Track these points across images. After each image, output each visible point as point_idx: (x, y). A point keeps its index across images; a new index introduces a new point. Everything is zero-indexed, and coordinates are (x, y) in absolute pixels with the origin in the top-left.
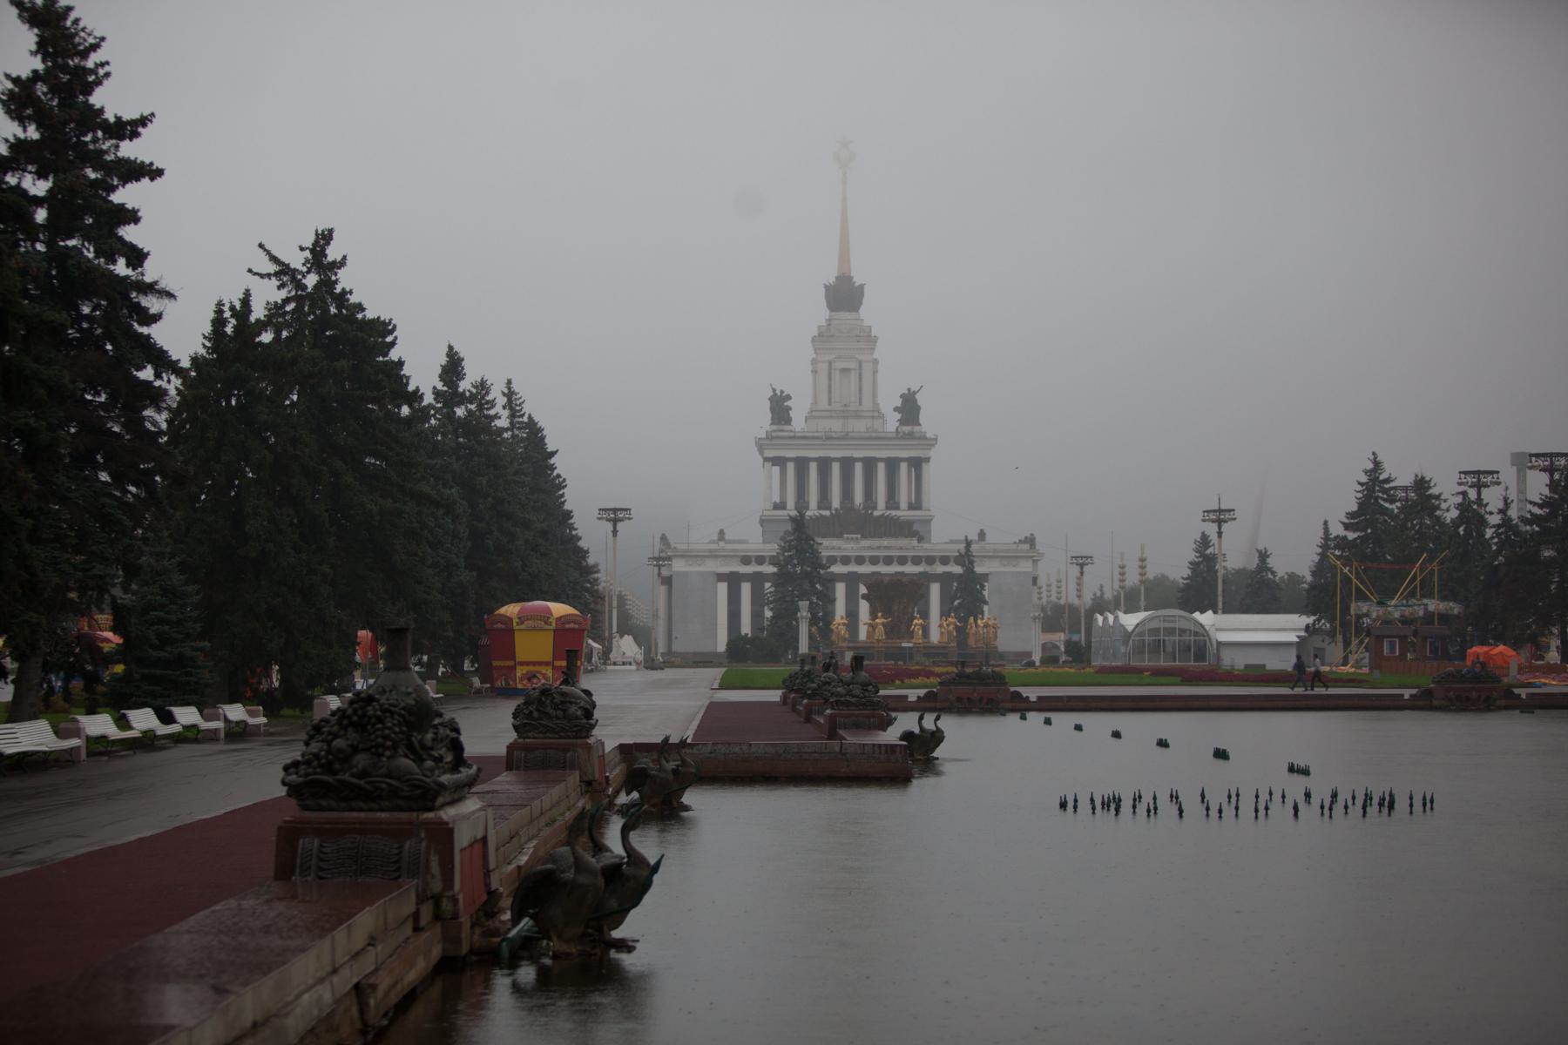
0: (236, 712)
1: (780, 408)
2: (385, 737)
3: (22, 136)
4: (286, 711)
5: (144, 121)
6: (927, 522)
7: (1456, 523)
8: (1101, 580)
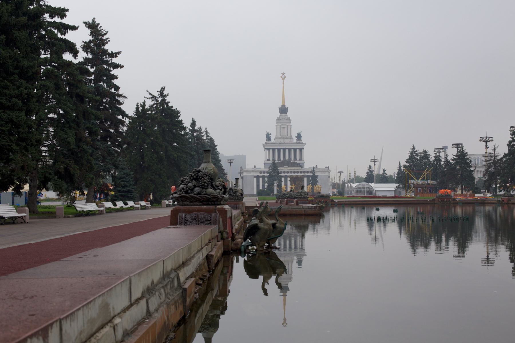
0: (143, 203)
1: (268, 137)
2: (205, 182)
3: (87, 57)
4: (155, 205)
5: (118, 53)
6: (303, 163)
7: (434, 161)
8: (345, 177)
